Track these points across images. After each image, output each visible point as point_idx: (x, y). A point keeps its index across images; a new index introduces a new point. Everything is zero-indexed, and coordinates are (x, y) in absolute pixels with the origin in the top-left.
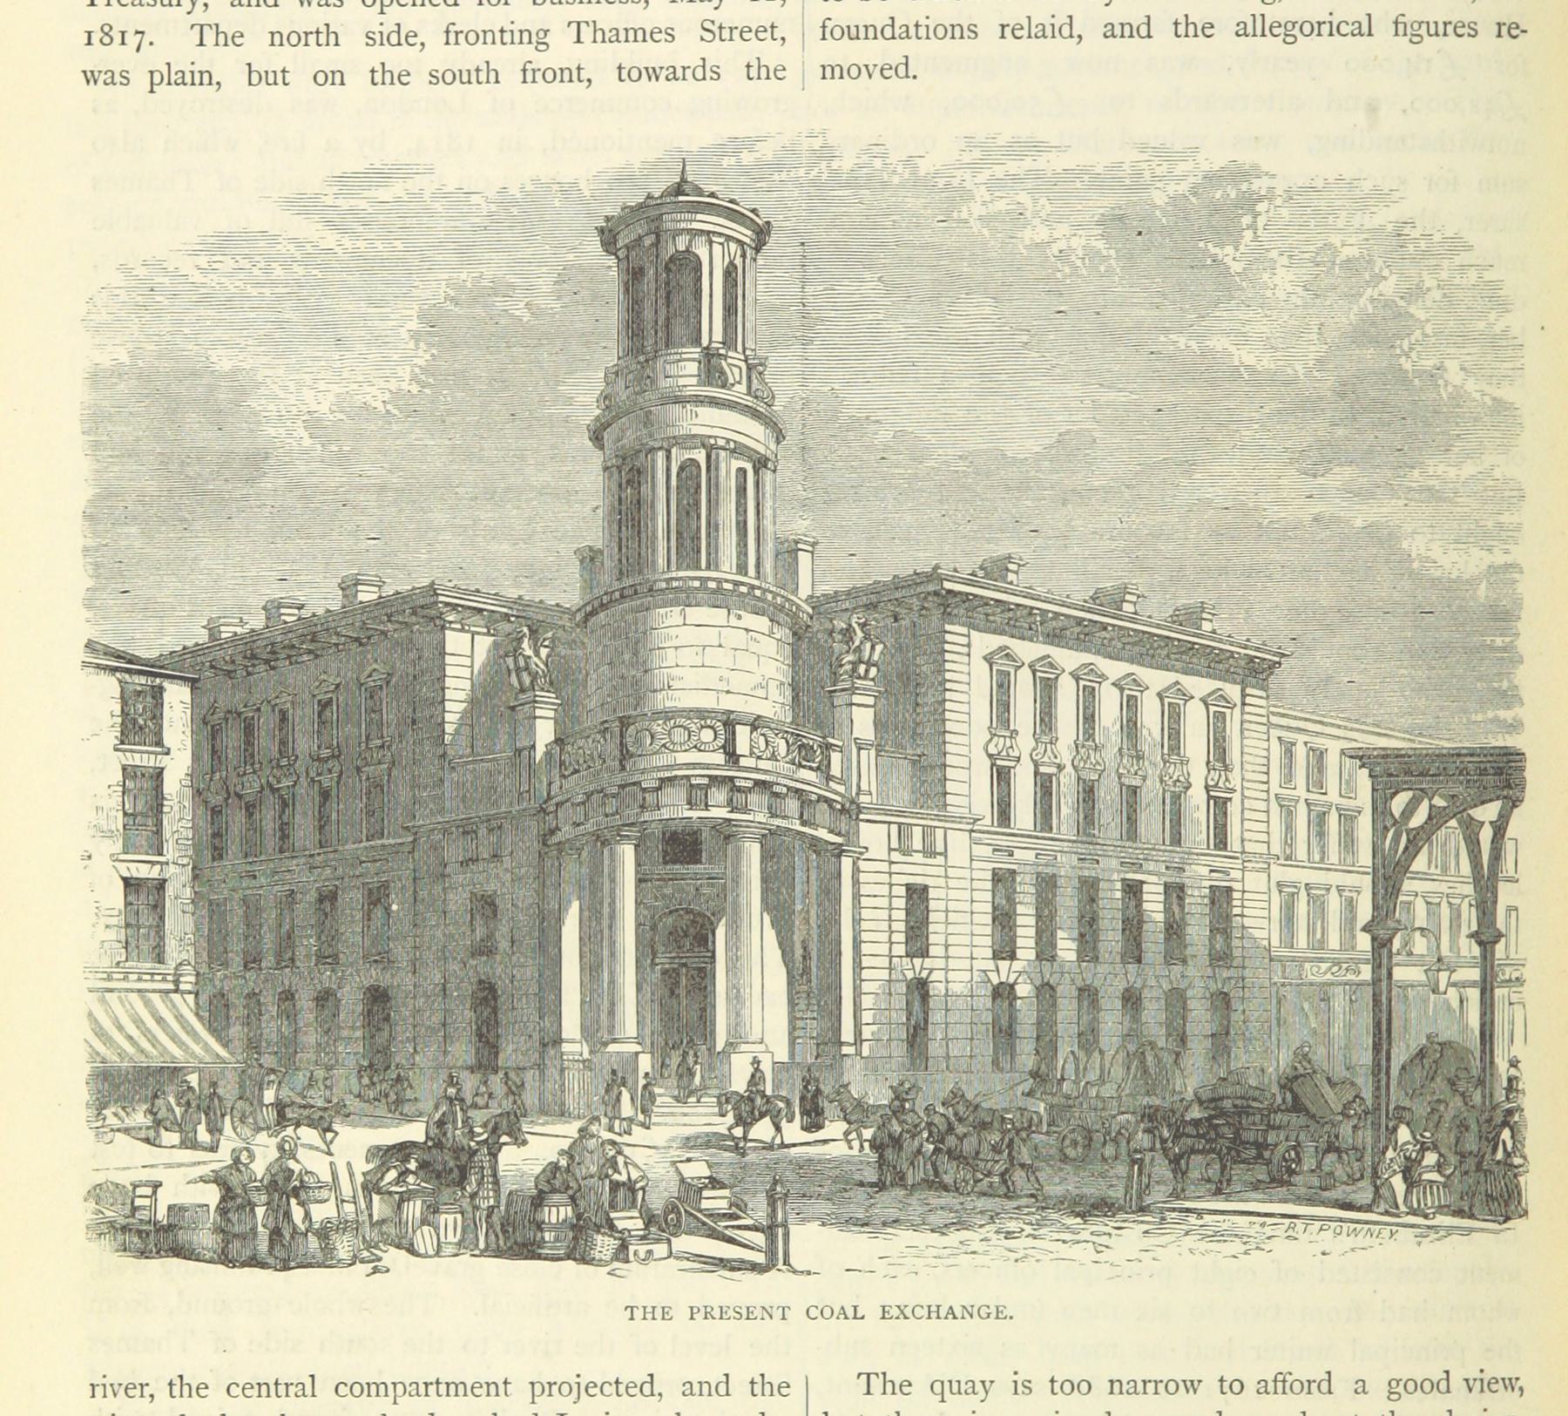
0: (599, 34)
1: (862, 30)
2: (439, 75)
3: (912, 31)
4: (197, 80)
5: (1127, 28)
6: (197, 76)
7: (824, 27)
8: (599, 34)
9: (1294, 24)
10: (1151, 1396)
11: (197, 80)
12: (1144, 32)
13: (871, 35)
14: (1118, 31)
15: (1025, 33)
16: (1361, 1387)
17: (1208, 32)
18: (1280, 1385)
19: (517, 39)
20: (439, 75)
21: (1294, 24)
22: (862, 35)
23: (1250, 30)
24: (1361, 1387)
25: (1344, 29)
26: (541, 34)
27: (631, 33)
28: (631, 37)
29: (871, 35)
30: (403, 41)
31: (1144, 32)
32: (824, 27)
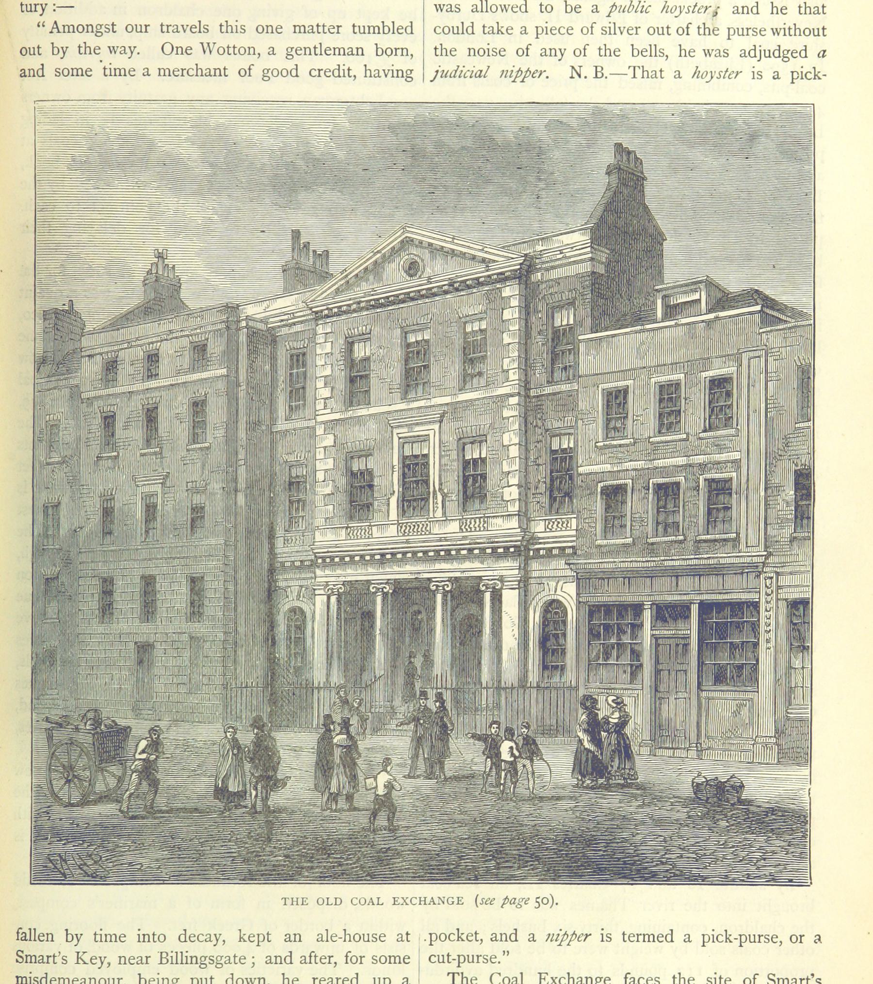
0: (645, 73)
1: (367, 29)
2: (378, 959)
3: (315, 29)
4: (189, 961)
5: (278, 959)
6: (189, 959)
7: (347, 956)
8: (645, 73)
9: (205, 958)
10: (641, 943)
11: (189, 961)
12: (40, 73)
13: (746, 11)
14: (548, 53)
15: (812, 76)
16: (688, 939)
17: (132, 73)
18: (313, 958)
19: (103, 939)
20: (378, 959)
21: (601, 978)
22: (367, 31)
23: (479, 9)
24: (688, 939)
25: (201, 938)
26: (409, 72)
27: (372, 29)
28: (108, 939)
29: (746, 11)
30: (187, 939)
31: (40, 73)
32: (347, 956)
